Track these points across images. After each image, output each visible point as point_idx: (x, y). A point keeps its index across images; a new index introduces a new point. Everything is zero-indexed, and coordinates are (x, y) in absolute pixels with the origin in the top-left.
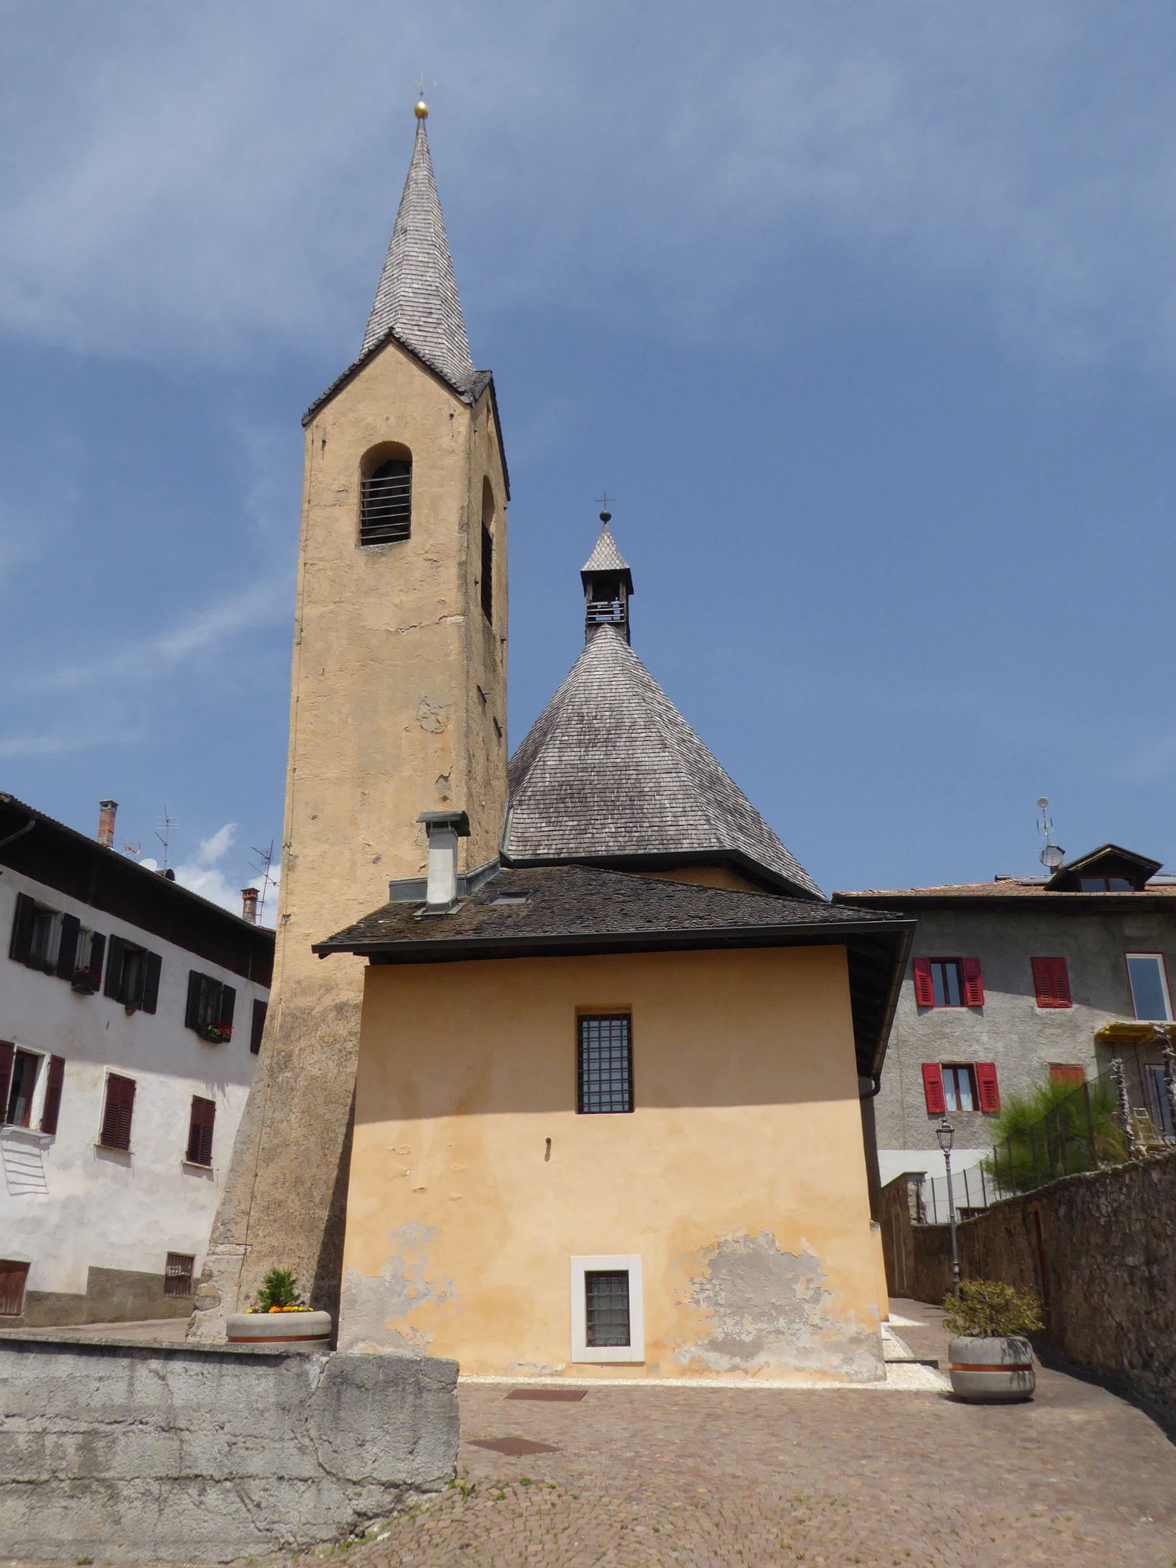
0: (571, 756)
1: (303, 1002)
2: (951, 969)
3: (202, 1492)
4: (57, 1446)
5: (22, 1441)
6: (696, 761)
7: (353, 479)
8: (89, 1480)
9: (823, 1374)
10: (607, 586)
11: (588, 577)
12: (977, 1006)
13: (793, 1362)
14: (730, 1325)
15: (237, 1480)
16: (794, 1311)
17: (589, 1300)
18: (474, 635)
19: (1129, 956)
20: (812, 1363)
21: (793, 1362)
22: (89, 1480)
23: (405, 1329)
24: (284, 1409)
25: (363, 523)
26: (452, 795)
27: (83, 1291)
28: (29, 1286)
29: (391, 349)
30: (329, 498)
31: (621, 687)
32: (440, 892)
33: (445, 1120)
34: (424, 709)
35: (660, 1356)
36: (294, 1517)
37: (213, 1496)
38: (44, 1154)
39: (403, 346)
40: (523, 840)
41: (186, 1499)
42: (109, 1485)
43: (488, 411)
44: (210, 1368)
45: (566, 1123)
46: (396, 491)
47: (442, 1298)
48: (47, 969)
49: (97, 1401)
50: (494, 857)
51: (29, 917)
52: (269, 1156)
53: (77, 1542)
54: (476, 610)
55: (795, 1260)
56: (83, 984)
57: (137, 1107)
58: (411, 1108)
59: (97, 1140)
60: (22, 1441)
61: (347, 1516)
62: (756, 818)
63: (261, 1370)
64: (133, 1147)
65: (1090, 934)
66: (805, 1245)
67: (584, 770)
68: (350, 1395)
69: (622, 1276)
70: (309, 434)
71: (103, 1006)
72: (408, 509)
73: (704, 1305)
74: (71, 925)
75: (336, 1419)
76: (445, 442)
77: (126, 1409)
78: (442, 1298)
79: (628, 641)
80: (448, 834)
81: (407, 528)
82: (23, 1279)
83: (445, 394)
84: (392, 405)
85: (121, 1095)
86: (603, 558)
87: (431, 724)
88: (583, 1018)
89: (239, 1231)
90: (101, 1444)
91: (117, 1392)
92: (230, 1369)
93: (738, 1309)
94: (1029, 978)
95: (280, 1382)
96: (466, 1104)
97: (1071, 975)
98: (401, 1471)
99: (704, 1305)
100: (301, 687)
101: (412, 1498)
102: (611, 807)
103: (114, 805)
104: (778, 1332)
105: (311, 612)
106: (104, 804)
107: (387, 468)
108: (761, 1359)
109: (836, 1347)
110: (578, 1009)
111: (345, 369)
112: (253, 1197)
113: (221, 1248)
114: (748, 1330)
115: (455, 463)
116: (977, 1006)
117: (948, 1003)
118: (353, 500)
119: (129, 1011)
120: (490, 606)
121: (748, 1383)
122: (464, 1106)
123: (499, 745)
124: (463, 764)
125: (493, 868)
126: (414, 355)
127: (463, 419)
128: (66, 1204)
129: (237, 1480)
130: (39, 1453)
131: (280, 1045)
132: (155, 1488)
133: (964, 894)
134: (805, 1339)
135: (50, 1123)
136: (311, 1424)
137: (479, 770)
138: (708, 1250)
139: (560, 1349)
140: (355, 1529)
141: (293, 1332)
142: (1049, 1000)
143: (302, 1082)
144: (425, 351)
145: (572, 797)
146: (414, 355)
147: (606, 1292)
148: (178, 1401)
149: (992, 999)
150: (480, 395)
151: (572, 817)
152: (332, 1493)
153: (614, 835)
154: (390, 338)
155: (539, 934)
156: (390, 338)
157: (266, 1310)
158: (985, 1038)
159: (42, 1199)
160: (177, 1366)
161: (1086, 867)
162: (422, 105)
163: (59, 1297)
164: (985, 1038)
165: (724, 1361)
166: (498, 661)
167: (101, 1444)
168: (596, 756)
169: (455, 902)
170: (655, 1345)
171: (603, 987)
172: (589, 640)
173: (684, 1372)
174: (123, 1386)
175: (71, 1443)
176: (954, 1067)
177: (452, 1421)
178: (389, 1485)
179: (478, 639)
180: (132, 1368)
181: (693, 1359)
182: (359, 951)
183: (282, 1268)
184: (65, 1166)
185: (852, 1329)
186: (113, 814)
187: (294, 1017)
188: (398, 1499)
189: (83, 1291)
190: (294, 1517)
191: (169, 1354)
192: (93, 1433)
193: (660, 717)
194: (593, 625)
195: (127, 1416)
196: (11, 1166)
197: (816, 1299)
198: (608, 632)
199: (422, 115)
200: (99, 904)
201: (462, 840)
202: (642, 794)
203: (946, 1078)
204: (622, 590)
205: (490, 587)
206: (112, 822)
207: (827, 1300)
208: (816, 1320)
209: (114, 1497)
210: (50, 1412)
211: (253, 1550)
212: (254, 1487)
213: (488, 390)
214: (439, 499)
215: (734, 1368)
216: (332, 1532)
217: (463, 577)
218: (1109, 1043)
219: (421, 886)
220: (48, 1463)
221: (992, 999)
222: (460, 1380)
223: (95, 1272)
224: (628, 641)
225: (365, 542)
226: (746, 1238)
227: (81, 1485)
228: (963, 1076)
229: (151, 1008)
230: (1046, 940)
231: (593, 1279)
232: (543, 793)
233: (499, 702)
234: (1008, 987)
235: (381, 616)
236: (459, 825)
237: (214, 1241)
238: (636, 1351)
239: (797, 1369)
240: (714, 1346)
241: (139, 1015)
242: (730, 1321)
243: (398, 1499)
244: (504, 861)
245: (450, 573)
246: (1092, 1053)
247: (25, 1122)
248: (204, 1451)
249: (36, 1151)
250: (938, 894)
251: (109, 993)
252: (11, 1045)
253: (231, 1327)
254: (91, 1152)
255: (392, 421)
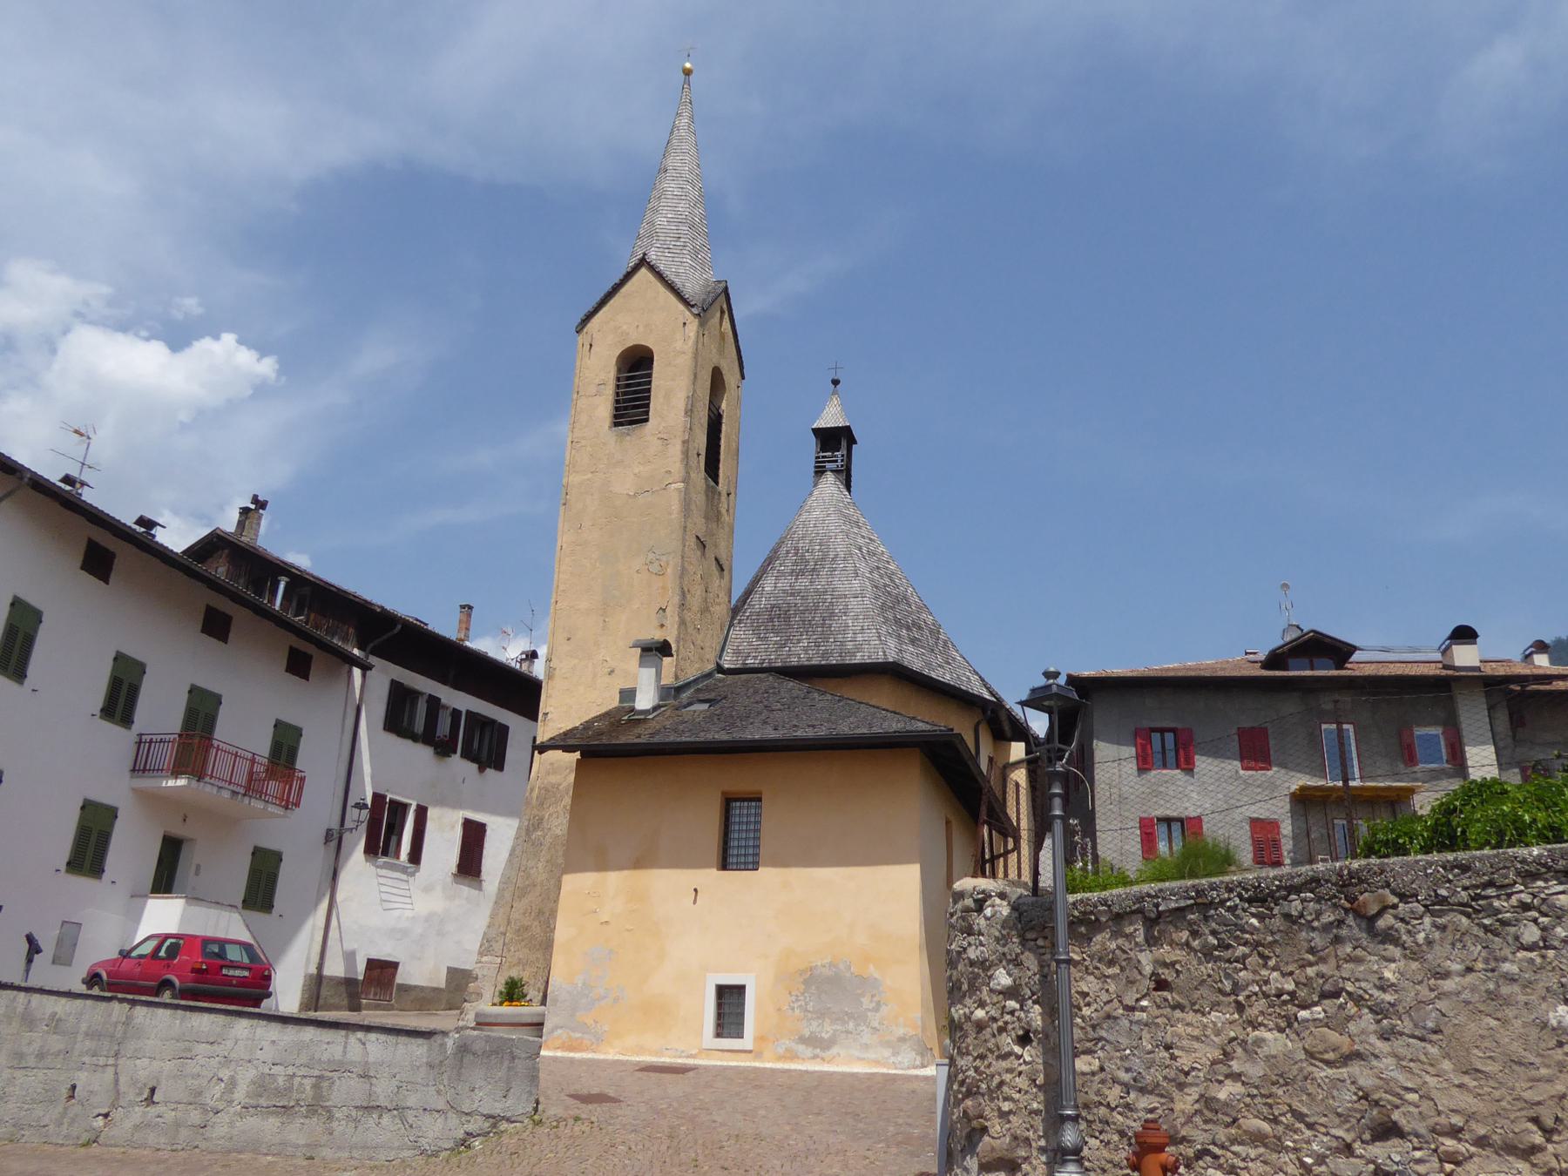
0: (783, 584)
1: (553, 779)
2: (1169, 737)
3: (380, 1117)
4: (301, 1084)
5: (281, 1081)
6: (886, 585)
7: (610, 374)
8: (317, 1107)
9: (877, 1062)
10: (834, 440)
11: (818, 432)
12: (1188, 768)
13: (857, 1053)
14: (814, 1025)
15: (400, 1110)
16: (860, 1018)
17: (719, 1005)
18: (694, 496)
19: (1324, 726)
20: (871, 1055)
21: (857, 1053)
22: (317, 1107)
23: (590, 1022)
24: (431, 1066)
25: (617, 409)
26: (668, 623)
27: (443, 985)
28: (399, 979)
29: (644, 272)
30: (592, 389)
31: (834, 523)
32: (645, 700)
33: (626, 873)
34: (651, 556)
35: (762, 1046)
36: (431, 1134)
37: (386, 1119)
38: (411, 879)
39: (652, 269)
40: (737, 652)
41: (371, 1120)
42: (328, 1110)
43: (722, 312)
44: (391, 1039)
45: (710, 878)
46: (639, 384)
47: (616, 1000)
48: (414, 738)
49: (325, 1057)
50: (711, 666)
51: (400, 698)
52: (522, 892)
53: (308, 1145)
54: (699, 476)
55: (865, 982)
56: (444, 749)
57: (487, 845)
58: (602, 864)
59: (454, 869)
60: (281, 1081)
61: (460, 1134)
62: (935, 632)
63: (420, 1041)
64: (484, 875)
65: (1290, 706)
66: (872, 971)
67: (792, 594)
68: (468, 1058)
69: (741, 989)
70: (580, 339)
71: (458, 764)
72: (648, 398)
73: (797, 1011)
74: (434, 703)
75: (459, 1074)
76: (679, 345)
77: (341, 1063)
78: (616, 1000)
79: (848, 487)
80: (653, 656)
81: (647, 413)
82: (394, 975)
83: (681, 307)
84: (645, 316)
85: (474, 835)
86: (831, 417)
87: (655, 568)
88: (728, 801)
89: (498, 946)
90: (325, 1084)
91: (336, 1051)
92: (403, 1039)
93: (821, 1015)
94: (1236, 744)
95: (430, 1050)
96: (641, 861)
97: (1272, 742)
98: (497, 1108)
99: (797, 1011)
100: (565, 538)
101: (504, 1126)
102: (807, 626)
103: (470, 608)
104: (848, 1032)
105: (574, 479)
106: (463, 607)
107: (636, 364)
108: (834, 1050)
109: (888, 1044)
110: (723, 793)
111: (608, 287)
112: (509, 922)
113: (485, 959)
114: (827, 1030)
115: (685, 361)
116: (1188, 768)
117: (1165, 766)
118: (609, 392)
119: (481, 769)
120: (717, 468)
121: (826, 1068)
122: (640, 863)
123: (722, 577)
124: (676, 599)
125: (709, 675)
126: (659, 275)
127: (693, 325)
128: (428, 918)
129: (400, 1110)
130: (290, 1089)
131: (535, 812)
132: (354, 1113)
133: (1180, 674)
134: (867, 1037)
135: (415, 857)
136: (445, 1076)
137: (695, 602)
138: (802, 972)
139: (693, 1039)
140: (465, 1142)
141: (516, 1020)
142: (1252, 764)
143: (548, 839)
144: (669, 274)
145: (779, 618)
146: (659, 275)
147: (730, 999)
148: (371, 1059)
149: (1202, 763)
150: (715, 305)
151: (777, 634)
152: (453, 1120)
153: (806, 649)
154: (643, 262)
155: (692, 739)
156: (643, 262)
157: (501, 1004)
158: (1194, 795)
159: (408, 914)
160: (373, 1036)
161: (1290, 650)
162: (688, 65)
163: (422, 988)
164: (1194, 795)
165: (809, 1052)
166: (723, 511)
167: (325, 1084)
168: (803, 582)
169: (655, 709)
170: (760, 1039)
171: (740, 778)
172: (816, 485)
173: (780, 1058)
174: (341, 1048)
175: (308, 1083)
176: (1168, 821)
177: (534, 1078)
178: (488, 1117)
179: (699, 499)
180: (347, 1037)
181: (787, 1050)
182: (568, 749)
183: (514, 973)
184: (428, 889)
185: (901, 1031)
186: (469, 615)
187: (547, 790)
188: (494, 1126)
189: (443, 985)
190: (431, 1134)
191: (369, 1029)
192: (320, 1077)
193: (860, 549)
194: (820, 472)
195: (340, 1067)
196: (384, 889)
197: (876, 1010)
198: (830, 478)
199: (687, 73)
200: (457, 686)
201: (667, 660)
202: (832, 614)
203: (1161, 830)
204: (844, 443)
205: (718, 453)
206: (468, 622)
207: (884, 1010)
208: (875, 1024)
209: (331, 1118)
210: (298, 1062)
211: (406, 1154)
212: (410, 1115)
213: (723, 297)
214: (672, 392)
215: (815, 1057)
216: (450, 1144)
217: (686, 454)
218: (1304, 801)
219: (628, 695)
220: (295, 1095)
221: (1202, 763)
222: (543, 1053)
223: (452, 972)
224: (848, 487)
225: (616, 424)
226: (831, 964)
227: (312, 1110)
228: (1176, 827)
229: (499, 765)
230: (1250, 714)
231: (722, 991)
232: (758, 614)
233: (723, 544)
234: (1216, 753)
235: (624, 484)
236: (664, 649)
237: (481, 954)
238: (747, 1042)
239: (860, 1059)
240: (803, 1040)
241: (490, 772)
242: (815, 1023)
243: (494, 1126)
244: (720, 669)
245: (676, 449)
246: (1288, 807)
247: (397, 856)
248: (383, 1090)
249: (404, 877)
250: (1172, 674)
251: (467, 755)
252: (384, 797)
253: (477, 1015)
254: (450, 879)
255: (641, 329)
